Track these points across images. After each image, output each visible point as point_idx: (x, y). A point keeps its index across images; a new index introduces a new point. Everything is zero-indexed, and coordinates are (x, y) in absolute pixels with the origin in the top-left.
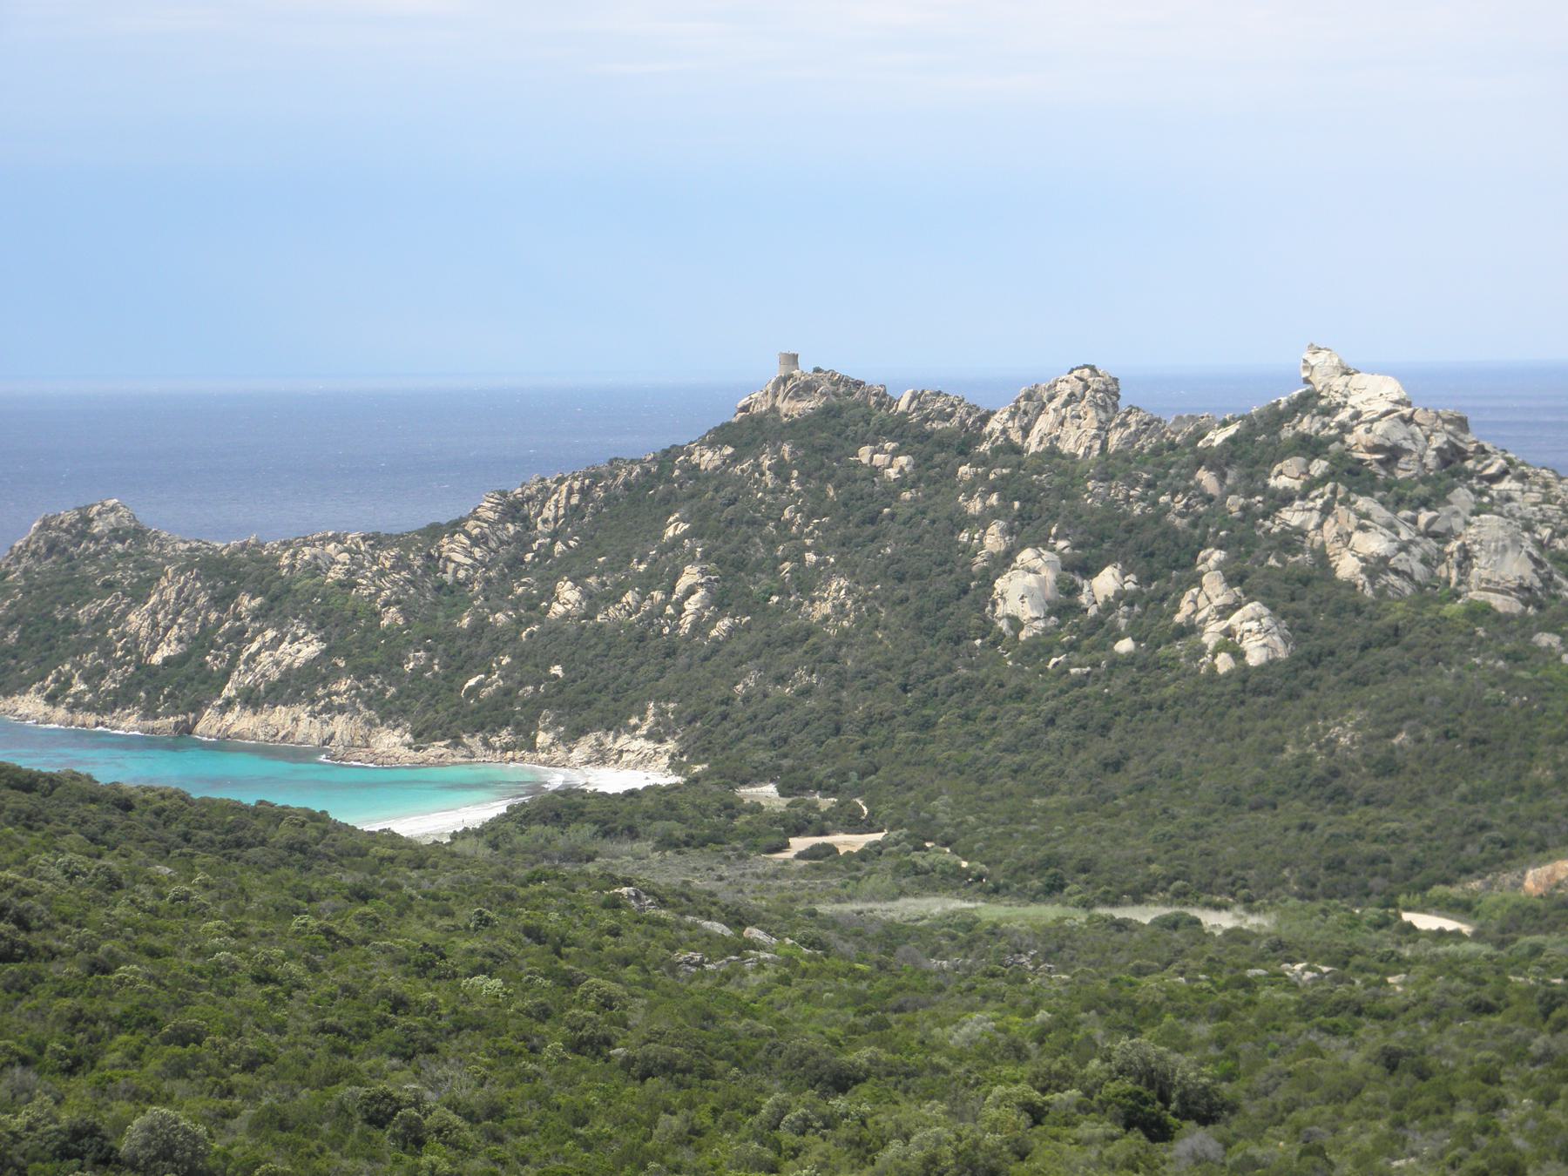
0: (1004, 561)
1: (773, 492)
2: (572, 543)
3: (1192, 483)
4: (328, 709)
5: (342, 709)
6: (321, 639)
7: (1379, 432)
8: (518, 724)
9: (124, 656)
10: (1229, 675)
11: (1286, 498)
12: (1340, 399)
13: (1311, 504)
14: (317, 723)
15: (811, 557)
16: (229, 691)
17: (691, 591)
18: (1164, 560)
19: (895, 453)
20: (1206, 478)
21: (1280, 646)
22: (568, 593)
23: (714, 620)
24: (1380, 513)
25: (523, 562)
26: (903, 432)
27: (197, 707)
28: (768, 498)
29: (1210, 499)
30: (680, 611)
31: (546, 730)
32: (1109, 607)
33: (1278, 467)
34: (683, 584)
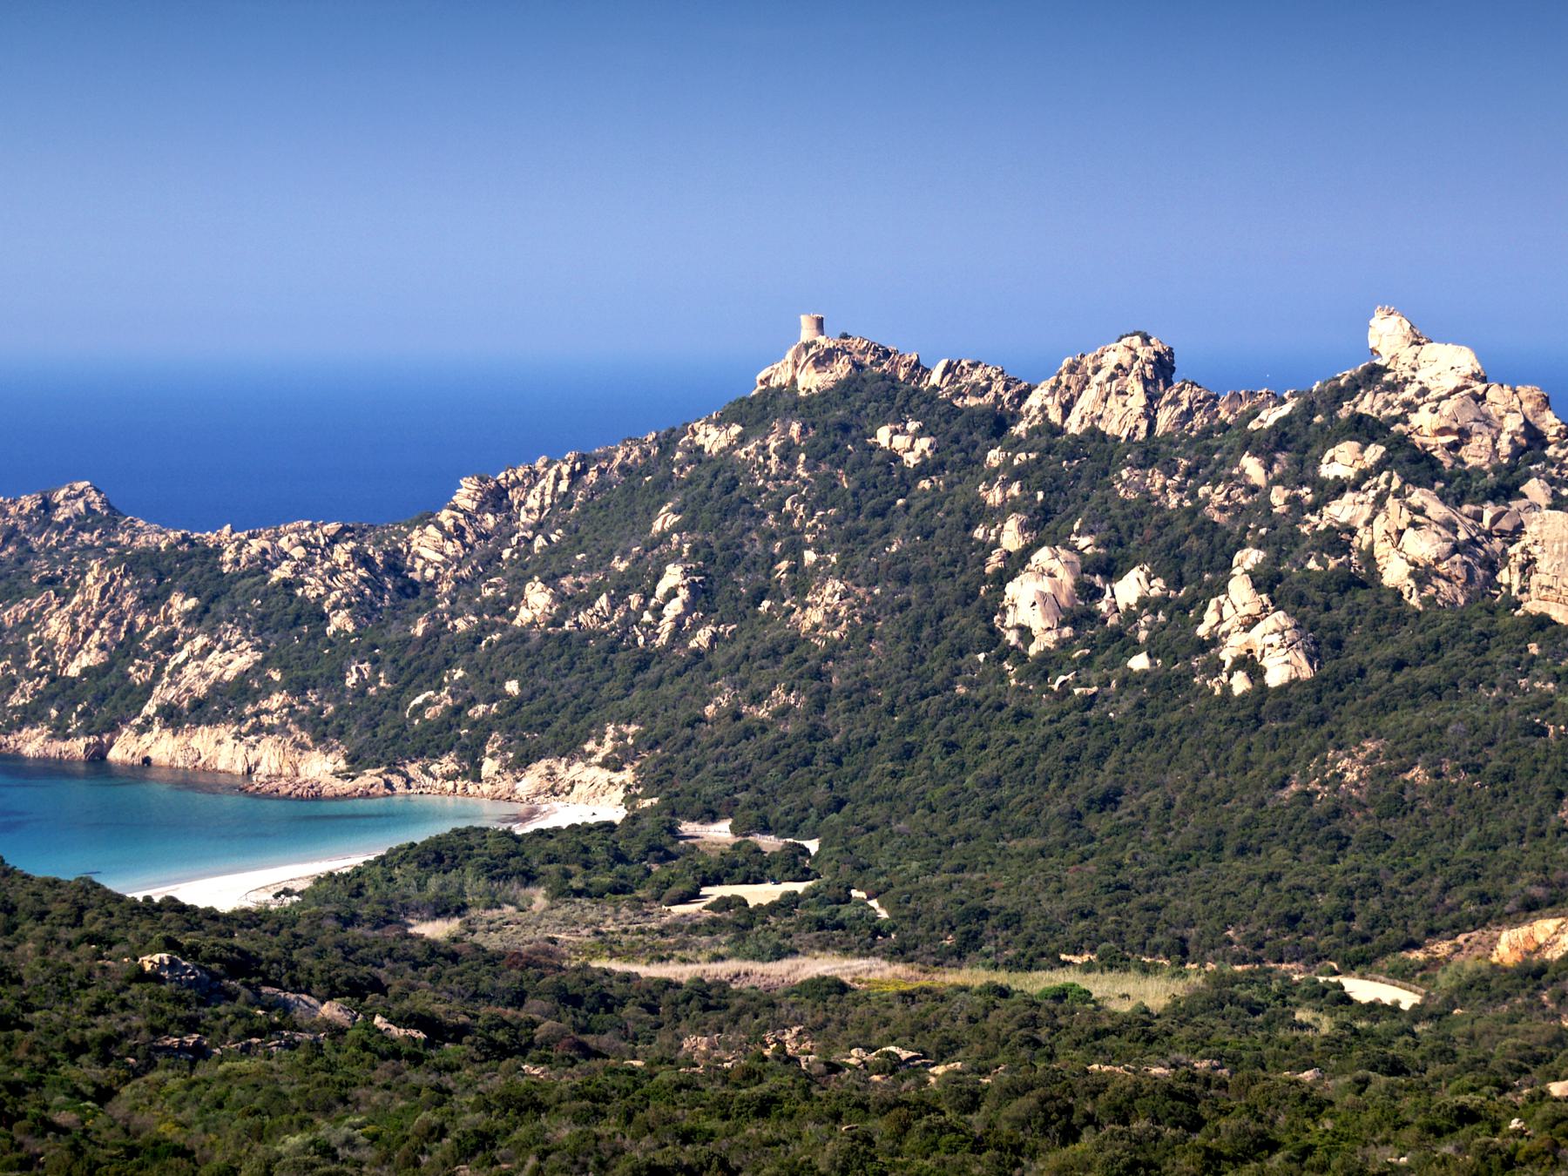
0: (1017, 563)
1: (776, 478)
2: (554, 537)
3: (1235, 471)
4: (257, 729)
5: (271, 730)
6: (256, 648)
7: (1446, 412)
8: (464, 748)
9: (39, 666)
10: (1244, 696)
11: (1339, 488)
12: (1408, 374)
13: (1362, 497)
14: (242, 748)
15: (810, 556)
16: (150, 709)
17: (672, 594)
18: (1195, 561)
19: (920, 433)
20: (1252, 467)
21: (1305, 665)
22: (537, 600)
23: (696, 626)
24: (1436, 510)
25: (500, 559)
26: (935, 413)
27: (113, 728)
28: (770, 485)
29: (1254, 489)
30: (658, 612)
31: (492, 756)
32: (1131, 616)
33: (1330, 453)
34: (662, 588)
